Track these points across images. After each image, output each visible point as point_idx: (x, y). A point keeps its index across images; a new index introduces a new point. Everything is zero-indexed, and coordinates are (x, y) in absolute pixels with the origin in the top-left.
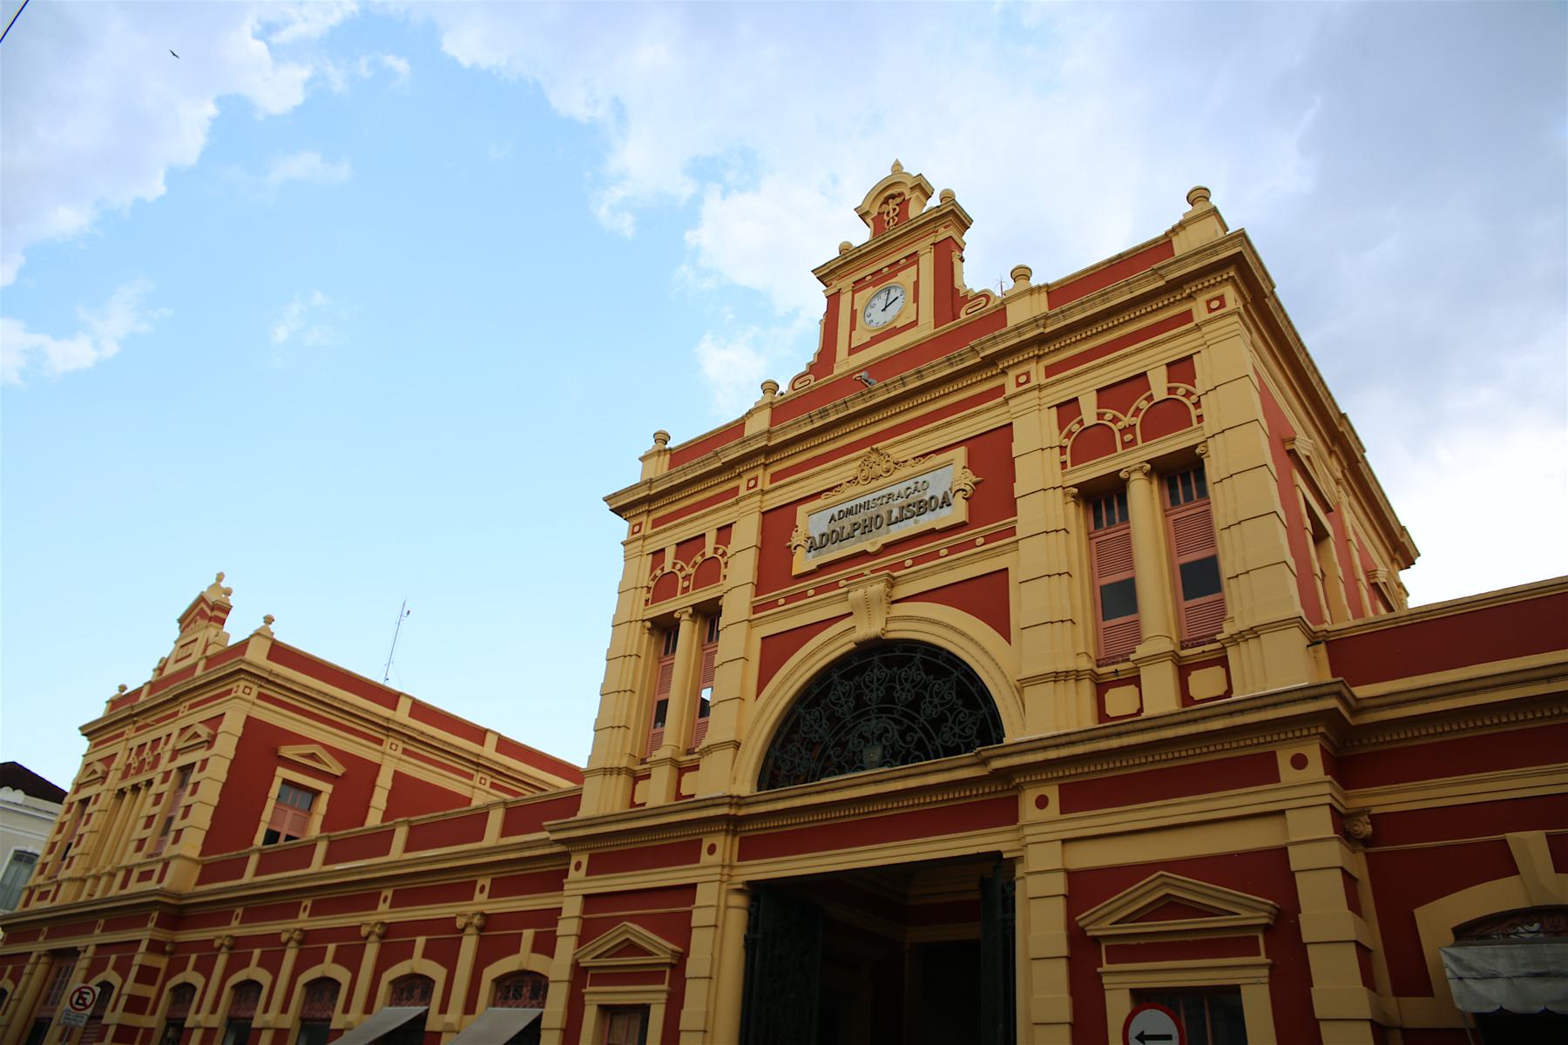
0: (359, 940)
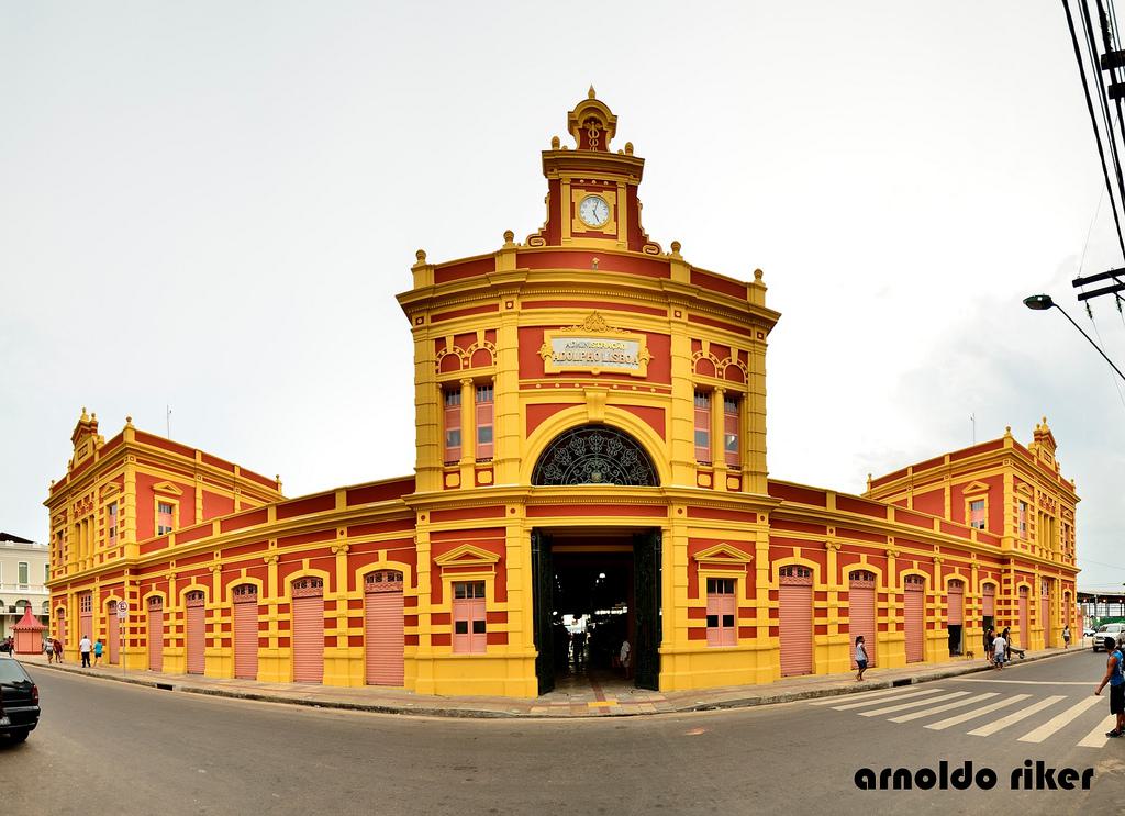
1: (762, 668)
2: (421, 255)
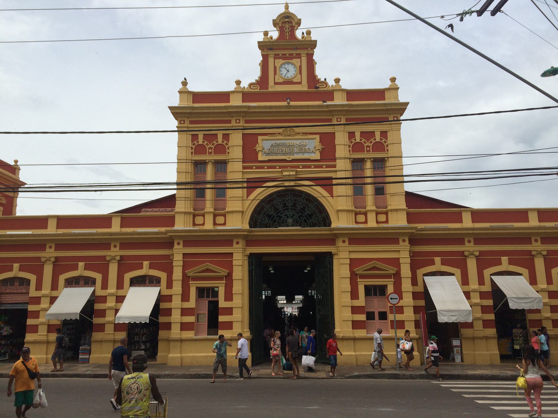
0: (41, 263)
1: (478, 353)
2: (185, 83)
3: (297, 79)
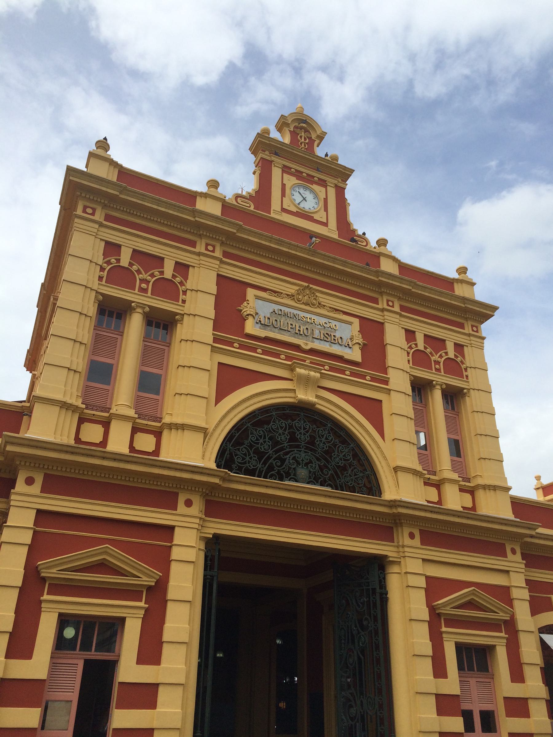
3: (321, 216)
